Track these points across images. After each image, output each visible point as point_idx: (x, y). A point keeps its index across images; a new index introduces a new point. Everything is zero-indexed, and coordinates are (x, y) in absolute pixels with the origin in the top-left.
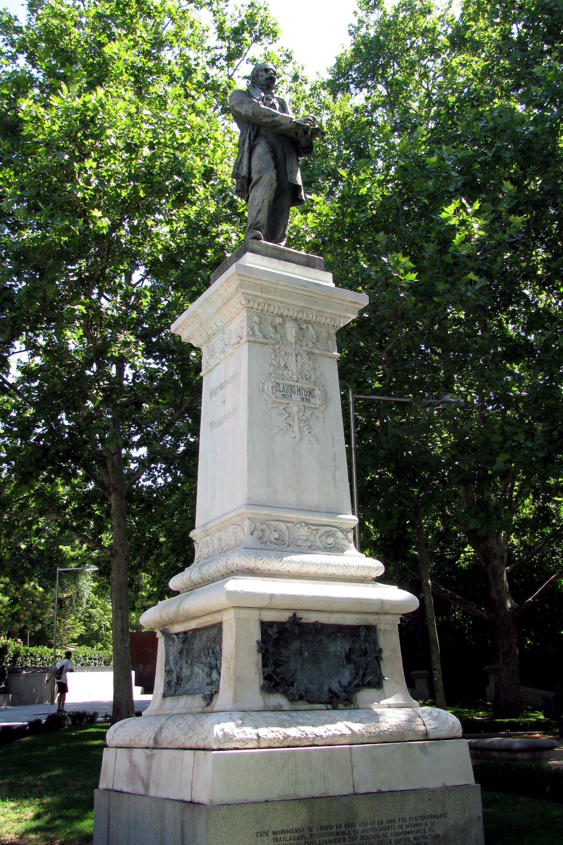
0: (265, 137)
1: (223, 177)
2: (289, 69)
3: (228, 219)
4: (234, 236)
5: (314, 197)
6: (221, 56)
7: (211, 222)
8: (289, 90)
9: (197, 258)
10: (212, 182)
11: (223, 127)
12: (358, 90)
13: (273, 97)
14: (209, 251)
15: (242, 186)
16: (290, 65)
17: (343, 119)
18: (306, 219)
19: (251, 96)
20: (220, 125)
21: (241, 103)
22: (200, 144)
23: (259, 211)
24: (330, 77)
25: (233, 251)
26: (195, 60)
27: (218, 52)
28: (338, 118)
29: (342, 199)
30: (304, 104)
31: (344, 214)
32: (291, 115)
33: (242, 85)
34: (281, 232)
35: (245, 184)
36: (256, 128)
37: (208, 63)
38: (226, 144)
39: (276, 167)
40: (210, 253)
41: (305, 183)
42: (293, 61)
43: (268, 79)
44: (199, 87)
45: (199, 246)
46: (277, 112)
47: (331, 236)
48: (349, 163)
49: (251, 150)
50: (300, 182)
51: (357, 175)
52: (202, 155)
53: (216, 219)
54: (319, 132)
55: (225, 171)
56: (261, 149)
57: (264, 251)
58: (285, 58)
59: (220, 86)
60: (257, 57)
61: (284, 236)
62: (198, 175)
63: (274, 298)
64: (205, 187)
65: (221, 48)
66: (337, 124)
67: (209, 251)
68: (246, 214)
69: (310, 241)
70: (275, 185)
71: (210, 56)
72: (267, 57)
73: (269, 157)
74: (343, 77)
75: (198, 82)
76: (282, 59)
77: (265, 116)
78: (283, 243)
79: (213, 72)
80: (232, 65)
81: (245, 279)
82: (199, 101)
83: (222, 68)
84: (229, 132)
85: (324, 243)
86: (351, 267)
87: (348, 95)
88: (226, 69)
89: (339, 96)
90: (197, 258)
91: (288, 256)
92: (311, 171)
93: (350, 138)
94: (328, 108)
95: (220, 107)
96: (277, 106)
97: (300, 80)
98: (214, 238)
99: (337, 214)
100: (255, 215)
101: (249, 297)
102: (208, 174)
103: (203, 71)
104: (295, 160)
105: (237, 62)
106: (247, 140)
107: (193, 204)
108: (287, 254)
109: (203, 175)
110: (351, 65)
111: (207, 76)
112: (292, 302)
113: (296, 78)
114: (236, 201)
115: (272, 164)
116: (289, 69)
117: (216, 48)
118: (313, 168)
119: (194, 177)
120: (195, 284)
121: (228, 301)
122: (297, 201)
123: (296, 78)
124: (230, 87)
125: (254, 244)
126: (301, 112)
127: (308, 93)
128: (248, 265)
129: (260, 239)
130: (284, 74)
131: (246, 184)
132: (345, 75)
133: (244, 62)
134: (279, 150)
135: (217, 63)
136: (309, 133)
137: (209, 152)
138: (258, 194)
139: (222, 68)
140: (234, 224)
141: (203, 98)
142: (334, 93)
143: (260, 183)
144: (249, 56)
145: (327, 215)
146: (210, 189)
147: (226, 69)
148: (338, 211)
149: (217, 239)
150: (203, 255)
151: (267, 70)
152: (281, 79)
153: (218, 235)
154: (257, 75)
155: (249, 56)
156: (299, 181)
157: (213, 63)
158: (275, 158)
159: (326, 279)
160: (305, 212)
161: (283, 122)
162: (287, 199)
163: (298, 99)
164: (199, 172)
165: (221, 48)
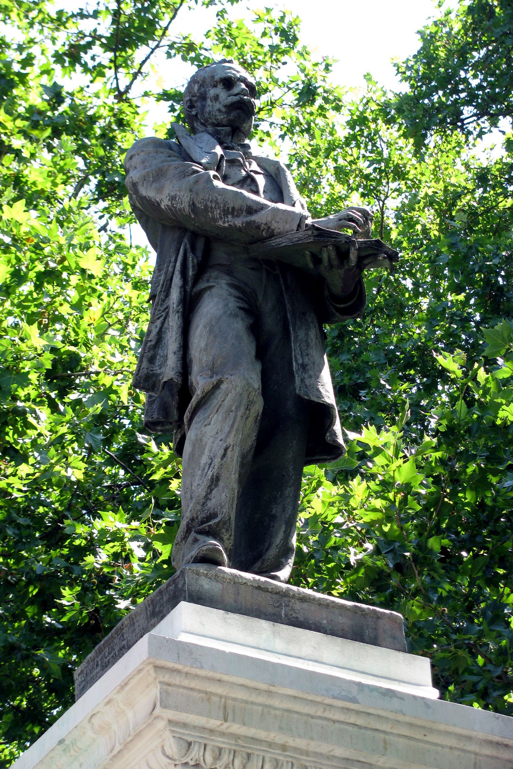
0: (229, 272)
1: (106, 380)
2: (289, 70)
3: (119, 500)
4: (137, 550)
5: (369, 436)
6: (96, 37)
7: (70, 507)
8: (290, 130)
9: (30, 611)
10: (74, 396)
11: (104, 237)
12: (485, 123)
13: (248, 156)
14: (66, 592)
15: (165, 409)
16: (292, 60)
17: (446, 204)
18: (346, 497)
19: (187, 157)
20: (94, 233)
21: (158, 176)
22: (38, 287)
23: (215, 481)
24: (405, 88)
25: (135, 595)
26: (20, 48)
27: (87, 26)
28: (431, 202)
29: (449, 436)
30: (331, 164)
31: (455, 480)
32: (299, 204)
33: (155, 120)
34: (278, 540)
35: (173, 404)
36: (200, 244)
37: (59, 58)
38: (113, 283)
39: (261, 355)
40: (68, 596)
41: (340, 391)
42: (299, 46)
43: (231, 107)
44: (35, 125)
45: (34, 579)
46: (261, 199)
47: (422, 547)
48: (464, 328)
49: (189, 306)
50: (328, 394)
51: (490, 365)
52: (45, 318)
53: (85, 500)
54: (377, 250)
55: (113, 364)
56: (216, 305)
57: (229, 598)
58: (276, 40)
59: (93, 120)
60: (198, 39)
61: (286, 550)
62: (33, 377)
63: (262, 735)
64: (54, 408)
65: (96, 14)
66: (427, 218)
67: (66, 592)
68: (175, 485)
69: (360, 563)
70: (259, 406)
71: (64, 38)
72: (225, 38)
73: (239, 326)
74: (442, 86)
75: (31, 109)
76: (266, 42)
77: (226, 212)
78: (285, 573)
79: (71, 80)
80: (127, 63)
81: (177, 680)
82: (35, 165)
83: (98, 71)
84: (119, 249)
85: (399, 568)
86: (481, 635)
87: (459, 135)
88: (110, 73)
89: (433, 139)
90: (30, 611)
91: (301, 610)
92: (357, 355)
93: (466, 258)
94: (399, 173)
95: (94, 181)
96: (261, 181)
97: (319, 101)
98: (80, 552)
99: (437, 481)
100: (201, 491)
101: (189, 735)
102: (64, 372)
103: (45, 80)
104: (313, 334)
105: (139, 53)
106: (177, 281)
107: (20, 457)
108: (298, 606)
109: (50, 376)
110: (463, 52)
111: (56, 95)
112: (314, 746)
113: (308, 94)
114: (143, 449)
115: (249, 347)
116: (289, 70)
117: (82, 15)
118: (363, 345)
119: (23, 380)
120: (22, 689)
121: (126, 746)
122: (324, 450)
123: (308, 94)
124: (121, 124)
125: (202, 578)
126: (325, 188)
127: (342, 132)
128: (184, 638)
129: (218, 563)
130: (277, 84)
131: (174, 403)
132: (449, 81)
133: (161, 53)
134: (267, 306)
135: (86, 58)
136: (353, 256)
137: (65, 310)
138: (210, 431)
139: (98, 71)
140: (135, 513)
141: (45, 156)
142: (417, 133)
143: (215, 402)
144: (175, 33)
145: (407, 488)
146: (70, 414)
147: (110, 73)
148: (439, 471)
149: (90, 559)
150: (47, 601)
151: (229, 83)
152: (264, 98)
153: (91, 547)
154: (203, 97)
155: (175, 33)
156: (327, 391)
157: (73, 55)
158: (255, 329)
159: (413, 676)
160: (342, 477)
161: (277, 226)
162: (292, 446)
163: (315, 152)
164: (38, 367)
165: (96, 14)
